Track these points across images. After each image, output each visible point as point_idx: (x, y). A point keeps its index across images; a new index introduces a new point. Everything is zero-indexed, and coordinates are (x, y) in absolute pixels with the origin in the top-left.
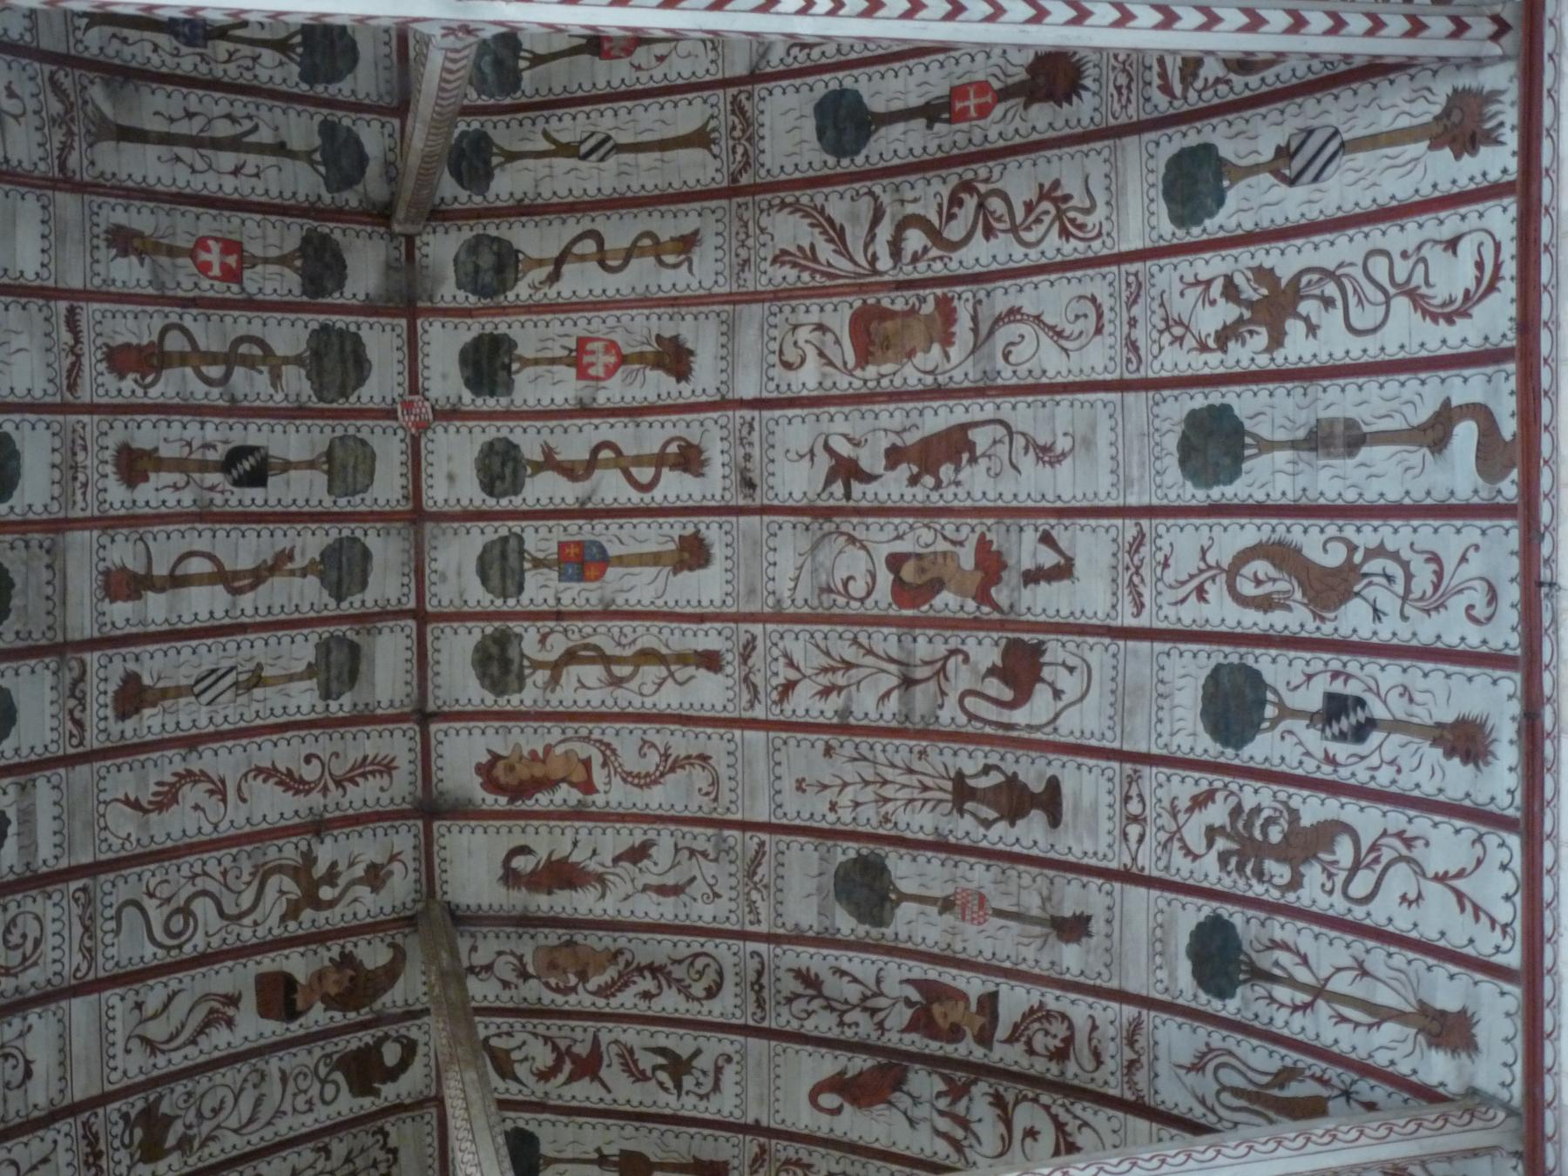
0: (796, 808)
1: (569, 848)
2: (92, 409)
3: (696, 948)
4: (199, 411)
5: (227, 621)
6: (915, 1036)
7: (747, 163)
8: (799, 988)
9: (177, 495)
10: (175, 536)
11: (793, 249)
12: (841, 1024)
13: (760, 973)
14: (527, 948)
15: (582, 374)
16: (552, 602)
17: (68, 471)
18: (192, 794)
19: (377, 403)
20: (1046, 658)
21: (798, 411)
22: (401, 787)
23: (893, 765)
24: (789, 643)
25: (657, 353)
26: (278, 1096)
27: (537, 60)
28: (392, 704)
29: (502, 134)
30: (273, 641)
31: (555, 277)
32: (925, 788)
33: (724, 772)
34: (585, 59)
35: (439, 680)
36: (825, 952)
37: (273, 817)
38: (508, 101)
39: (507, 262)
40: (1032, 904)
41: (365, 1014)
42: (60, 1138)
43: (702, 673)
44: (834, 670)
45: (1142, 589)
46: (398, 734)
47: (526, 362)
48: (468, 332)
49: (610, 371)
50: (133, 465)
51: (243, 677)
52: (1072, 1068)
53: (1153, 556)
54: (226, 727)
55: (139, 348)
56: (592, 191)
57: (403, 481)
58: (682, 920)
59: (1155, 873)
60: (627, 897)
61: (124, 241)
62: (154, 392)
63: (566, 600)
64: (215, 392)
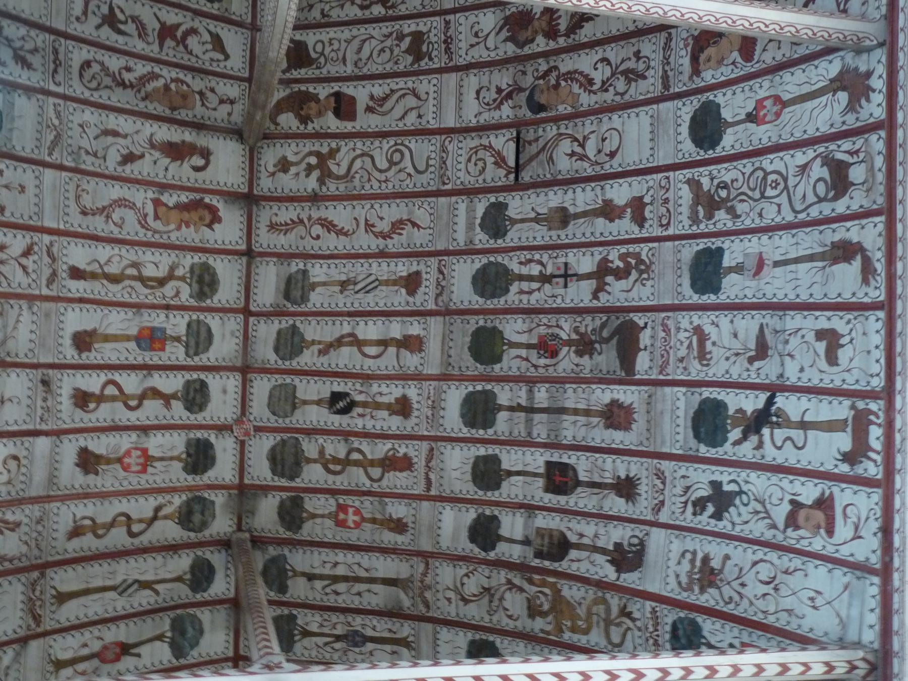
0: (26, 175)
1: (170, 169)
2: (422, 438)
3: (96, 94)
4: (366, 435)
5: (358, 319)
7: (33, 585)
8: (29, 57)
9: (380, 390)
10: (383, 368)
11: (6, 532)
13: (55, 71)
14: (199, 110)
15: (145, 451)
16: (171, 316)
17: (436, 406)
18: (383, 226)
21: (10, 428)
22: (265, 215)
24: (25, 281)
25: (98, 464)
27: (160, 638)
29: (183, 592)
31: (158, 509)
33: (72, 203)
34: (131, 641)
35: (239, 274)
36: (11, 78)
37: (340, 207)
38: (179, 612)
39: (185, 517)
41: (296, 87)
42: (464, 56)
43: (82, 266)
46: (265, 246)
47: (178, 458)
48: (210, 476)
49: (128, 453)
50: (403, 407)
51: (351, 287)
54: (362, 261)
55: (395, 470)
56: (132, 561)
58: (104, 113)
60: (137, 132)
61: (399, 526)
62: (389, 446)
63: (162, 316)
64: (356, 445)
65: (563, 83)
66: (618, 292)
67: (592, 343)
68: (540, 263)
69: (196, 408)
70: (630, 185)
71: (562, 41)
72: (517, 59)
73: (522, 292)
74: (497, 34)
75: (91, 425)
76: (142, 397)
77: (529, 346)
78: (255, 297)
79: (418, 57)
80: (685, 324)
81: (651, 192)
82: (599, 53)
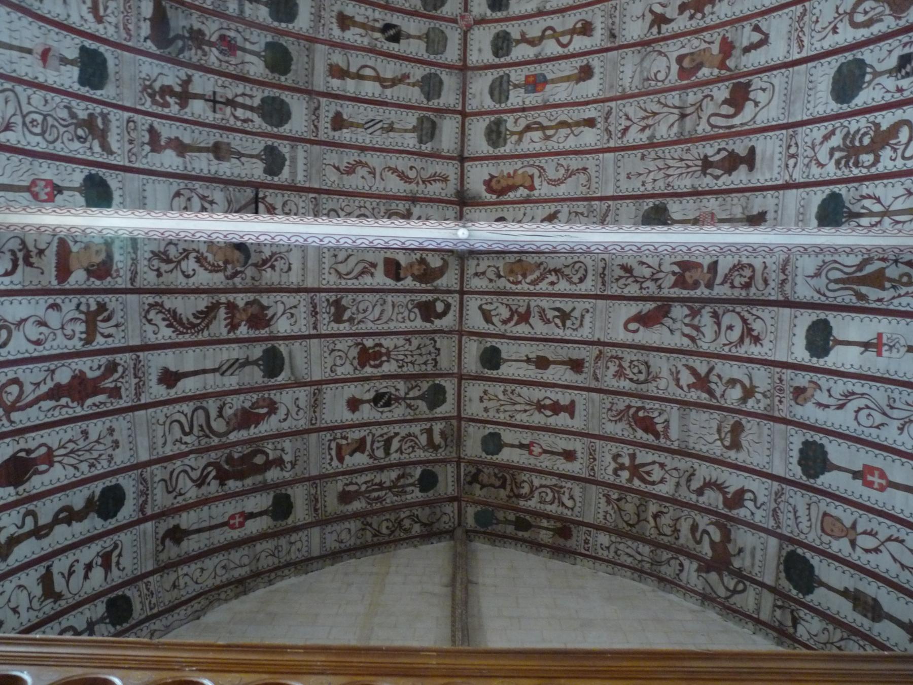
0: (626, 187)
3: (576, 259)
6: (676, 289)
8: (622, 273)
9: (362, 39)
12: (641, 288)
13: (604, 269)
14: (500, 264)
16: (521, 103)
19: (449, 15)
20: (752, 88)
22: (449, 190)
23: (673, 159)
26: (390, 313)
28: (448, 151)
30: (399, 112)
32: (688, 167)
33: (593, 174)
35: (469, 143)
40: (738, 212)
41: (429, 287)
44: (647, 117)
45: (804, 38)
46: (450, 165)
51: (385, 126)
52: (753, 290)
53: (810, 19)
54: (377, 146)
57: (459, 52)
59: (802, 180)
65: (221, 263)
66: (171, 76)
67: (190, 38)
68: (235, 117)
69: (501, 35)
70: (162, 164)
71: (223, 298)
72: (261, 291)
73: (251, 97)
74: (275, 314)
75: (580, 10)
76: (542, 38)
77: (244, 50)
78: (457, 125)
79: (337, 303)
80: (111, 30)
81: (144, 153)
82: (193, 283)
